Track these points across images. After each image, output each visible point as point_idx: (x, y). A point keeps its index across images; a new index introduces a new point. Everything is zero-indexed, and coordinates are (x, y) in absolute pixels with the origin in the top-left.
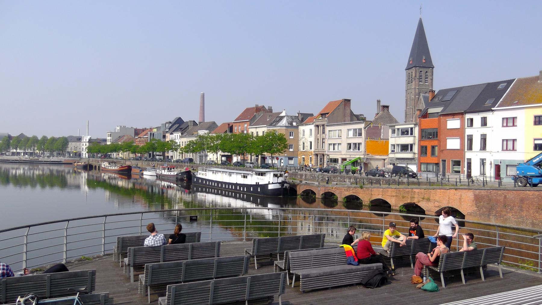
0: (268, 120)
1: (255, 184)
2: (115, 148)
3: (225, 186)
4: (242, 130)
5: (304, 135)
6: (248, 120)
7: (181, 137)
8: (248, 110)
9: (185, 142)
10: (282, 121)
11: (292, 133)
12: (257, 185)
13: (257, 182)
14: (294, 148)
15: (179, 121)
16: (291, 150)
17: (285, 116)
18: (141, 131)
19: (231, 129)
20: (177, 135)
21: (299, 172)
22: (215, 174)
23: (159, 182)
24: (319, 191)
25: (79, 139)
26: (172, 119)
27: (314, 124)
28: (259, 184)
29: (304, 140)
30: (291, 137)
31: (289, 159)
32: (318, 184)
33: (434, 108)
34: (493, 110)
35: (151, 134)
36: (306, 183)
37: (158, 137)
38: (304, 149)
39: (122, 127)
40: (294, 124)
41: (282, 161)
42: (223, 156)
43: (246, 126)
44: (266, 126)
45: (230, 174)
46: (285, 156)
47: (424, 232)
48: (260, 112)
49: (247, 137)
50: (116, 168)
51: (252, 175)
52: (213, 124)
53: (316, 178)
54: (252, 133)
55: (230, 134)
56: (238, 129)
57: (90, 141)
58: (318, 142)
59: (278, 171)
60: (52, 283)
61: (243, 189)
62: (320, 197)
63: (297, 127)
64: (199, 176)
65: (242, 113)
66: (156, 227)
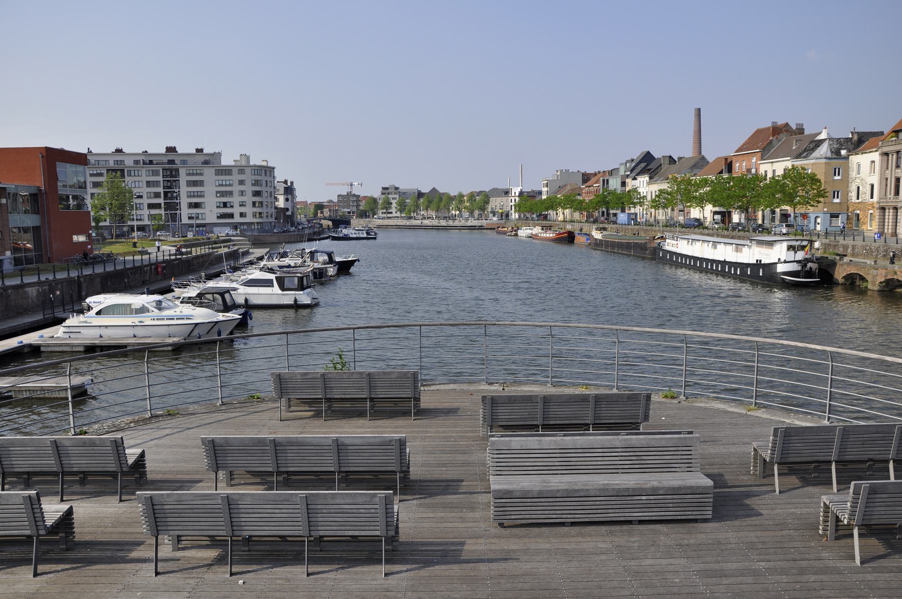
0: (794, 148)
1: (755, 262)
2: (552, 204)
3: (707, 265)
4: (748, 168)
5: (859, 173)
7: (649, 184)
8: (759, 132)
9: (656, 191)
10: (819, 148)
11: (839, 169)
12: (759, 265)
13: (759, 259)
14: (841, 196)
15: (648, 157)
16: (836, 201)
17: (826, 139)
18: (592, 176)
19: (729, 167)
20: (644, 179)
21: (842, 242)
22: (692, 245)
24: (874, 276)
25: (507, 193)
26: (636, 154)
27: (880, 151)
28: (762, 262)
29: (859, 181)
30: (837, 178)
31: (831, 217)
32: (873, 263)
35: (604, 180)
36: (851, 261)
37: (614, 184)
38: (858, 199)
39: (564, 171)
40: (843, 152)
41: (819, 220)
42: (715, 213)
43: (754, 160)
44: (789, 158)
45: (715, 244)
46: (824, 211)
48: (781, 135)
49: (757, 178)
50: (551, 235)
51: (750, 247)
53: (872, 252)
54: (766, 172)
55: (726, 176)
56: (741, 167)
57: (521, 194)
58: (887, 185)
59: (797, 240)
60: (596, 412)
61: (736, 270)
62: (876, 288)
63: (847, 158)
64: (667, 248)
65: (749, 139)
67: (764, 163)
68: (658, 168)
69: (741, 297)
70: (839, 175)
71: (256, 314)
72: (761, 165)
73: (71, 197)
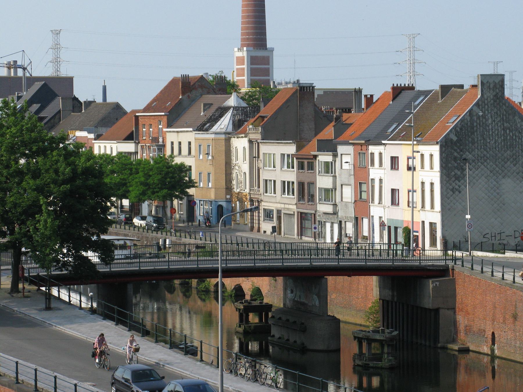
0: (202, 114)
6: (163, 114)
23: (7, 264)
33: (287, 143)
34: (384, 144)
44: (191, 129)
47: (457, 290)
52: (114, 109)
66: (140, 349)
67: (170, 132)
68: (53, 117)
69: (494, 377)
70: (372, 154)
71: (414, 150)
72: (167, 134)
73: (286, 155)
